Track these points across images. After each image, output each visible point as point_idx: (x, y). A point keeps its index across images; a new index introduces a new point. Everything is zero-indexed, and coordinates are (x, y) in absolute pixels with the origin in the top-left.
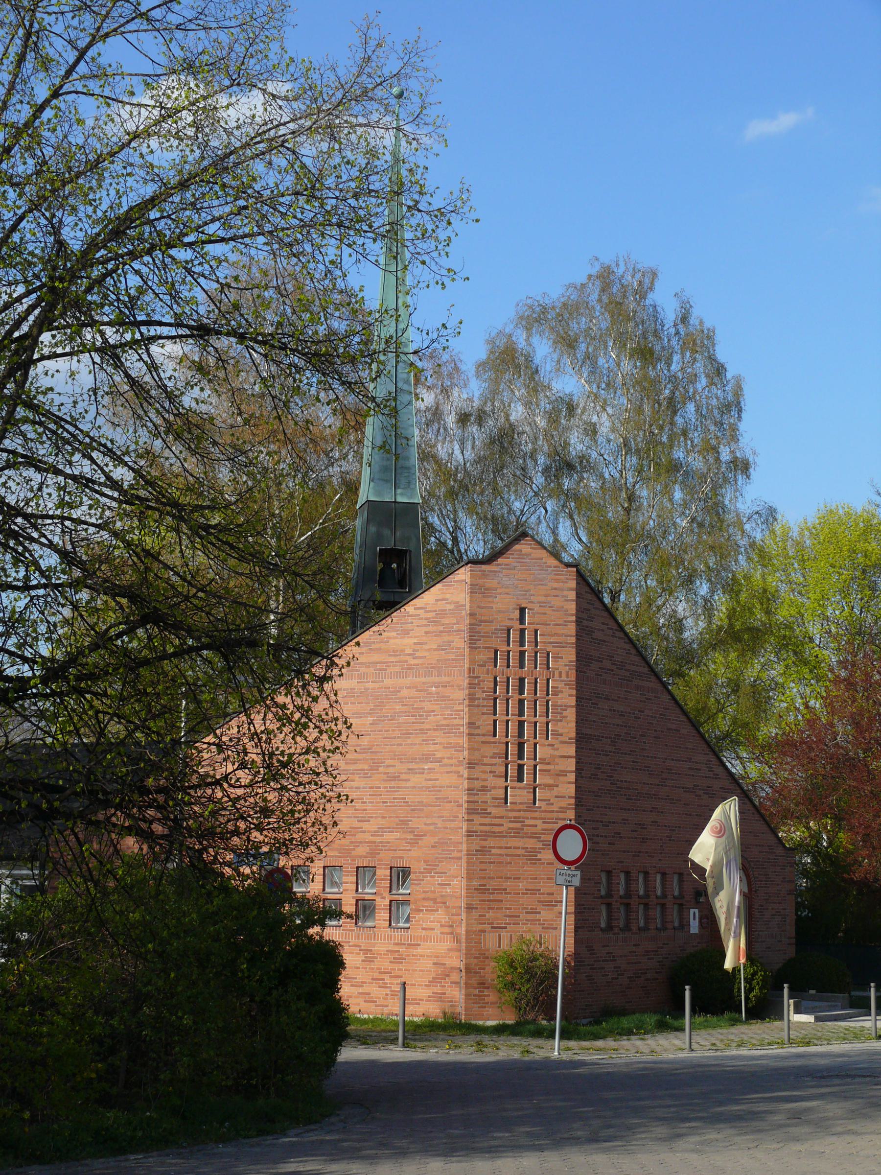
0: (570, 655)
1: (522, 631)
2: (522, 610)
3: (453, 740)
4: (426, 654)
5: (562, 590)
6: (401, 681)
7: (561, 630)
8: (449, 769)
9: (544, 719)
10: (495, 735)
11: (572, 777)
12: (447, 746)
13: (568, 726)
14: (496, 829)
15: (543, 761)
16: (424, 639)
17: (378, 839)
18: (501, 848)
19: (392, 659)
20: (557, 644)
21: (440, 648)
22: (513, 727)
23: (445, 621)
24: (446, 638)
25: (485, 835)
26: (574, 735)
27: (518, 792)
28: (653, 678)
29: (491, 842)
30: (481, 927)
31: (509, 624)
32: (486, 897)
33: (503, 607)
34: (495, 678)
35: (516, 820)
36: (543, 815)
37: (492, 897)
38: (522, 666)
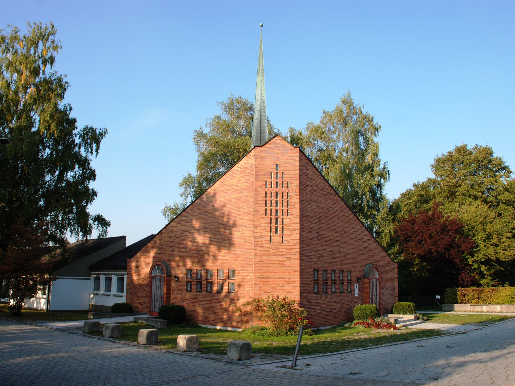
0: (297, 182)
1: (277, 173)
2: (277, 165)
3: (250, 217)
4: (241, 185)
5: (293, 157)
6: (232, 196)
7: (293, 173)
8: (249, 229)
9: (286, 208)
10: (266, 215)
11: (298, 231)
12: (248, 220)
13: (296, 210)
14: (267, 253)
15: (286, 225)
16: (240, 179)
17: (224, 258)
18: (268, 260)
19: (230, 188)
20: (292, 178)
21: (246, 182)
22: (274, 212)
23: (248, 171)
24: (248, 178)
25: (262, 255)
26: (299, 214)
27: (275, 238)
28: (337, 196)
29: (264, 258)
30: (261, 293)
31: (271, 171)
32: (263, 280)
33: (269, 164)
34: (266, 193)
35: (275, 249)
36: (286, 247)
37: (265, 280)
38: (277, 187)
